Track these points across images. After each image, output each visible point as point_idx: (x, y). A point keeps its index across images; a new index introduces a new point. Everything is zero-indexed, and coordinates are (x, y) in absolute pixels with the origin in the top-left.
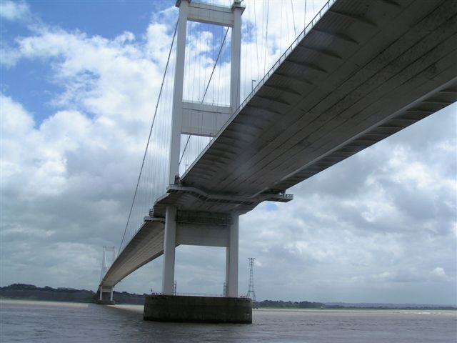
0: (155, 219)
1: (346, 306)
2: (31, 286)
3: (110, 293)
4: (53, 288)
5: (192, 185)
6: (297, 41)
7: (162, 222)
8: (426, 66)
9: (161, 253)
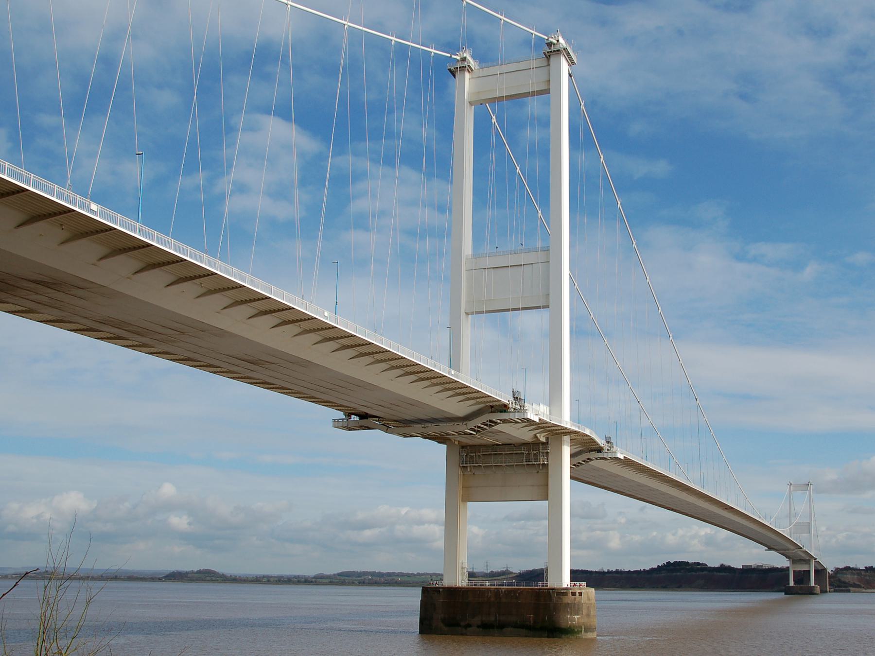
2: (698, 564)
4: (717, 566)
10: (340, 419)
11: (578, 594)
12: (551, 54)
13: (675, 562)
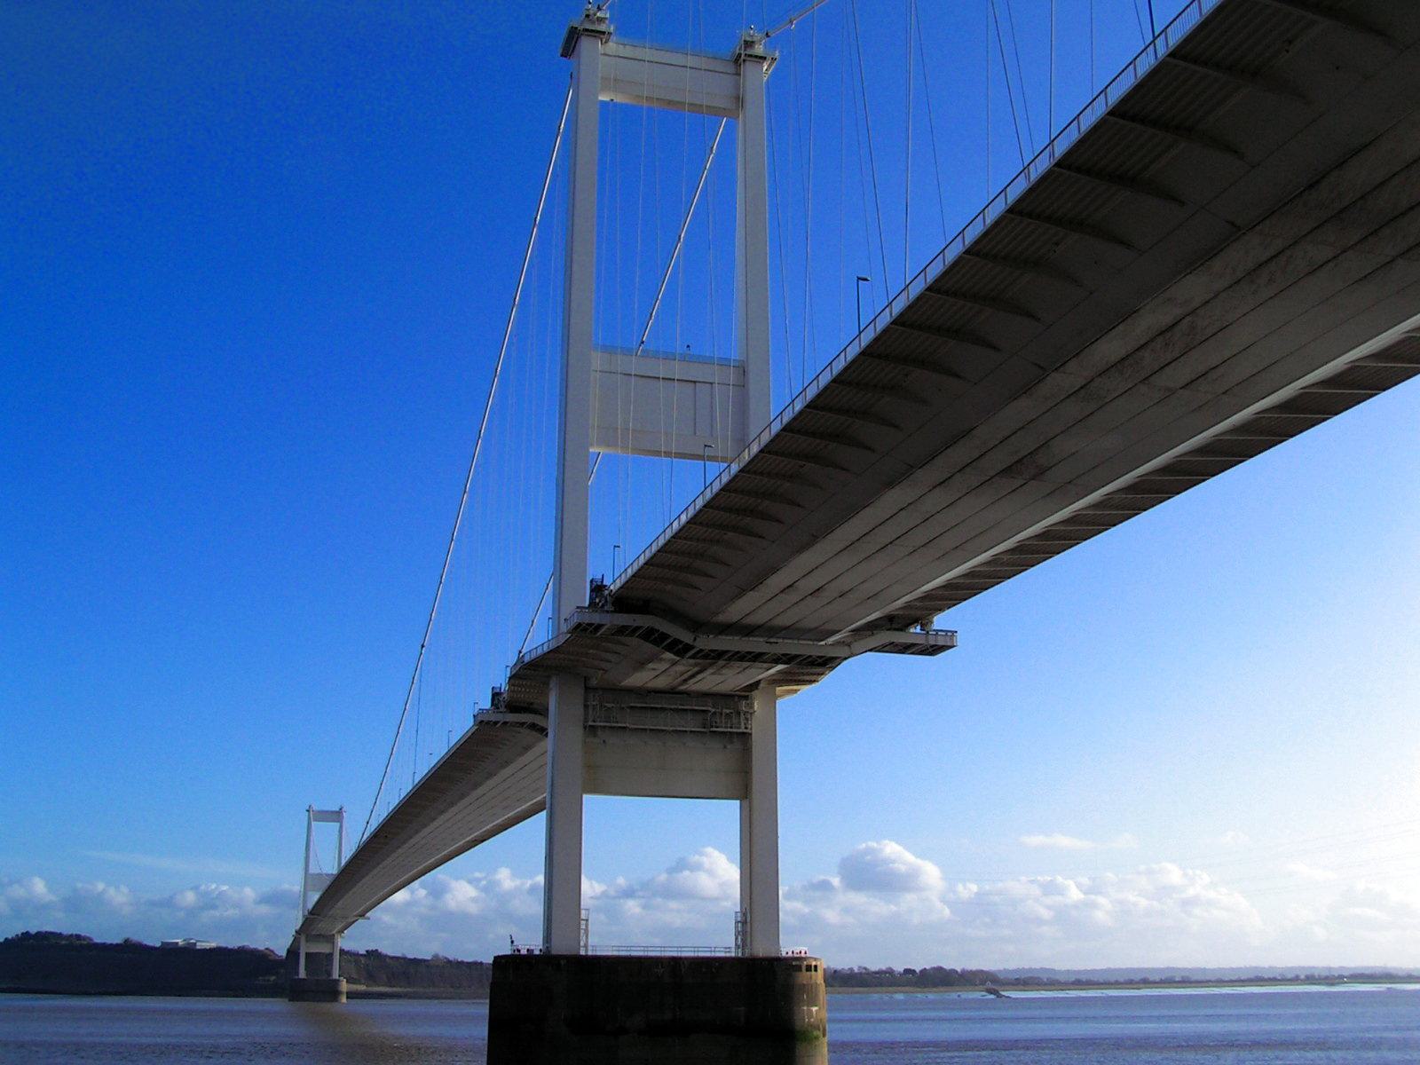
0: (511, 717)
1: (1062, 978)
2: (78, 937)
3: (331, 955)
4: (115, 942)
5: (643, 607)
6: (904, 294)
7: (533, 727)
8: (1367, 273)
9: (545, 809)
10: (941, 631)
11: (804, 968)
12: (749, 59)
13: (39, 933)
